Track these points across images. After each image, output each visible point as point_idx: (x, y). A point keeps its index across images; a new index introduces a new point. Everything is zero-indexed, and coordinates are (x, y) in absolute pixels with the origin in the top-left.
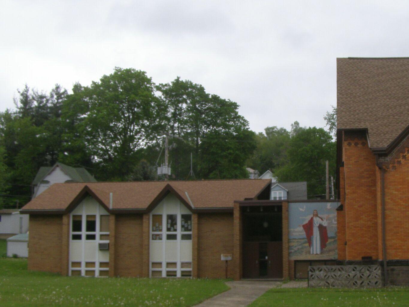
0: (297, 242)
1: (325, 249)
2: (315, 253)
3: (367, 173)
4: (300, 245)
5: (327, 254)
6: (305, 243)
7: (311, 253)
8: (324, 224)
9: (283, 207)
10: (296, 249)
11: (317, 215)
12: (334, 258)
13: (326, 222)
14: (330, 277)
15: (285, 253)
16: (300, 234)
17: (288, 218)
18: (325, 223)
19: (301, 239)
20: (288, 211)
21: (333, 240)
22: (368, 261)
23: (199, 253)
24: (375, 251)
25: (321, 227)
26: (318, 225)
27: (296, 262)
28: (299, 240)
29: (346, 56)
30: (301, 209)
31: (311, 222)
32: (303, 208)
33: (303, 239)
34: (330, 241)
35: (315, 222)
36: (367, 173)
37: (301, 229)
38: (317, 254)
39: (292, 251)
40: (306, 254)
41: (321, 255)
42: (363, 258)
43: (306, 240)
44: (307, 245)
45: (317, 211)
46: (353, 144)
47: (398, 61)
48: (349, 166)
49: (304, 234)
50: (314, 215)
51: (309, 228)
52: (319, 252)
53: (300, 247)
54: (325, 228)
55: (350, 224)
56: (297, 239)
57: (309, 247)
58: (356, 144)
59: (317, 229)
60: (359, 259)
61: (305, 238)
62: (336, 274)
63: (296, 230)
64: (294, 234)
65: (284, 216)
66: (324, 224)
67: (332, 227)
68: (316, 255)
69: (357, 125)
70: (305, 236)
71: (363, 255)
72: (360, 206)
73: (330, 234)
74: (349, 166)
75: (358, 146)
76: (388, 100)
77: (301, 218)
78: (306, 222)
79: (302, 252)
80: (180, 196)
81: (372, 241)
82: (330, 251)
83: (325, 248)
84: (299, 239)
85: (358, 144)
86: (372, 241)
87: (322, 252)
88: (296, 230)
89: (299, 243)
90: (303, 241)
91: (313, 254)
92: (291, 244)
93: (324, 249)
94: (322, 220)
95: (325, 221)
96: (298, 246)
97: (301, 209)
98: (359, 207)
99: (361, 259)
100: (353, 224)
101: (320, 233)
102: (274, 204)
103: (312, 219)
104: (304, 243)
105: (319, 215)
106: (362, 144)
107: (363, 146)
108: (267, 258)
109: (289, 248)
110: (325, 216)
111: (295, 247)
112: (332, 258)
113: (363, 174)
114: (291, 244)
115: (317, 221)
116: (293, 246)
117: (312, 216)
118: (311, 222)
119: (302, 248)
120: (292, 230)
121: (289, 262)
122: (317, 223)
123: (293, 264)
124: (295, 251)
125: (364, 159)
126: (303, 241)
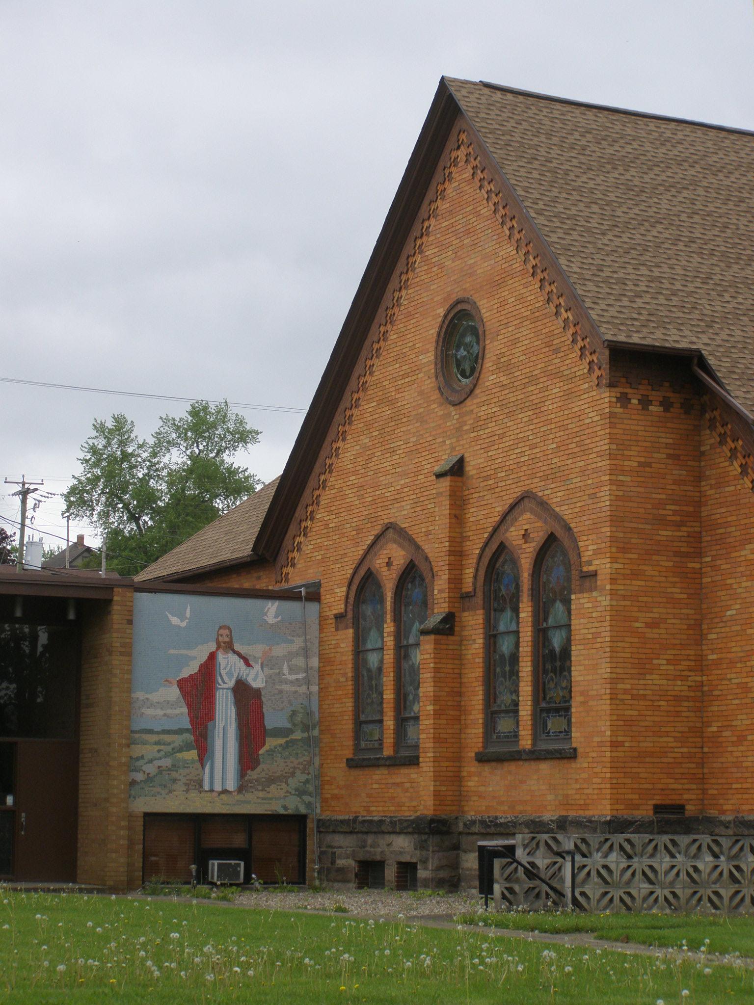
0: (157, 743)
1: (252, 775)
2: (218, 787)
3: (677, 508)
4: (166, 756)
5: (261, 794)
6: (186, 747)
7: (206, 787)
8: (255, 680)
9: (116, 608)
10: (151, 769)
11: (229, 647)
12: (285, 808)
13: (260, 672)
14: (639, 874)
15: (93, 786)
16: (169, 711)
17: (128, 652)
18: (256, 679)
19: (168, 732)
20: (130, 622)
21: (282, 741)
22: (672, 819)
23: (493, 761)
24: (694, 787)
25: (243, 693)
26: (232, 683)
27: (152, 819)
28: (167, 738)
29: (475, 77)
30: (175, 621)
31: (209, 667)
32: (182, 617)
33: (180, 731)
34: (271, 743)
35: (223, 672)
36: (677, 508)
37: (174, 692)
38: (225, 792)
39: (139, 777)
40: (187, 791)
41: (240, 797)
42: (658, 809)
43: (190, 737)
44: (193, 754)
45: (229, 629)
46: (634, 401)
47: (641, 122)
48: (621, 478)
49: (181, 715)
50: (218, 648)
51: (199, 690)
52: (231, 785)
53: (167, 762)
54: (258, 693)
55: (620, 686)
56: (158, 733)
57: (198, 765)
58: (645, 403)
59: (230, 695)
60: (645, 812)
61: (187, 730)
62: (655, 865)
63: (154, 697)
64: (149, 712)
65: (114, 638)
66: (255, 680)
67: (281, 692)
68: (223, 796)
69: (659, 334)
70: (186, 723)
71: (657, 800)
72: (653, 624)
73: (274, 718)
74: (621, 478)
75: (651, 408)
76: (696, 258)
77: (172, 651)
78: (192, 668)
79: (174, 781)
80: (313, 467)
81: (685, 750)
82: (272, 780)
83: (253, 769)
84: (165, 732)
85: (650, 402)
86: (685, 750)
87: (241, 789)
88: (154, 697)
89: (162, 747)
90: (178, 740)
91: (212, 791)
92: (138, 750)
93: (249, 772)
94: (248, 664)
95: (257, 667)
96: (160, 758)
97: (175, 621)
98: (648, 625)
99: (651, 813)
100: (628, 687)
101: (238, 714)
102: (12, 591)
103: (212, 657)
104: (181, 750)
105: (237, 647)
106: (661, 404)
107: (664, 411)
108: (10, 800)
109: (132, 764)
110: (255, 650)
111: (151, 761)
112: (276, 807)
113: (664, 512)
114: (138, 750)
115: (229, 668)
116: (142, 757)
117: (212, 647)
118: (209, 667)
119: (175, 767)
120: (139, 695)
121: (131, 816)
122: (230, 674)
123: (139, 825)
124: (149, 779)
125: (669, 456)
126: (178, 740)
